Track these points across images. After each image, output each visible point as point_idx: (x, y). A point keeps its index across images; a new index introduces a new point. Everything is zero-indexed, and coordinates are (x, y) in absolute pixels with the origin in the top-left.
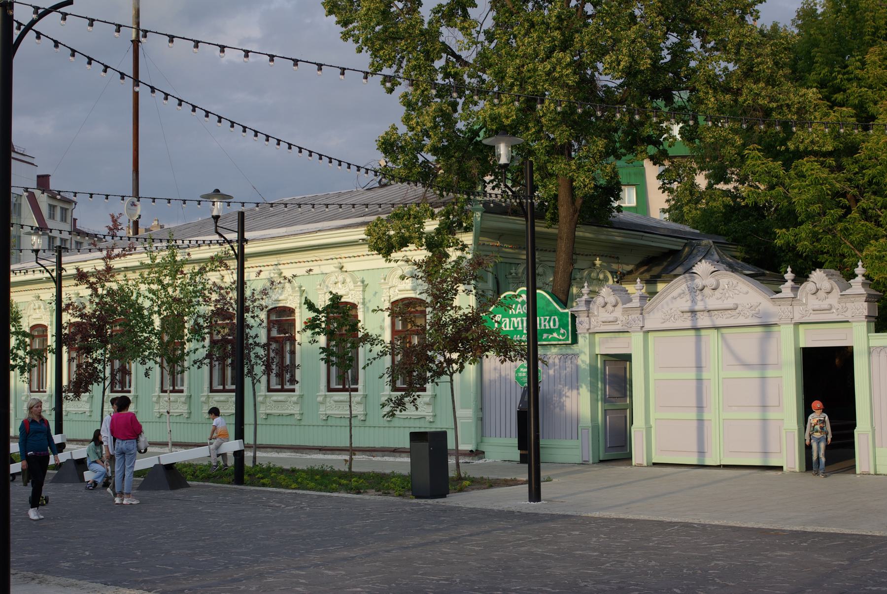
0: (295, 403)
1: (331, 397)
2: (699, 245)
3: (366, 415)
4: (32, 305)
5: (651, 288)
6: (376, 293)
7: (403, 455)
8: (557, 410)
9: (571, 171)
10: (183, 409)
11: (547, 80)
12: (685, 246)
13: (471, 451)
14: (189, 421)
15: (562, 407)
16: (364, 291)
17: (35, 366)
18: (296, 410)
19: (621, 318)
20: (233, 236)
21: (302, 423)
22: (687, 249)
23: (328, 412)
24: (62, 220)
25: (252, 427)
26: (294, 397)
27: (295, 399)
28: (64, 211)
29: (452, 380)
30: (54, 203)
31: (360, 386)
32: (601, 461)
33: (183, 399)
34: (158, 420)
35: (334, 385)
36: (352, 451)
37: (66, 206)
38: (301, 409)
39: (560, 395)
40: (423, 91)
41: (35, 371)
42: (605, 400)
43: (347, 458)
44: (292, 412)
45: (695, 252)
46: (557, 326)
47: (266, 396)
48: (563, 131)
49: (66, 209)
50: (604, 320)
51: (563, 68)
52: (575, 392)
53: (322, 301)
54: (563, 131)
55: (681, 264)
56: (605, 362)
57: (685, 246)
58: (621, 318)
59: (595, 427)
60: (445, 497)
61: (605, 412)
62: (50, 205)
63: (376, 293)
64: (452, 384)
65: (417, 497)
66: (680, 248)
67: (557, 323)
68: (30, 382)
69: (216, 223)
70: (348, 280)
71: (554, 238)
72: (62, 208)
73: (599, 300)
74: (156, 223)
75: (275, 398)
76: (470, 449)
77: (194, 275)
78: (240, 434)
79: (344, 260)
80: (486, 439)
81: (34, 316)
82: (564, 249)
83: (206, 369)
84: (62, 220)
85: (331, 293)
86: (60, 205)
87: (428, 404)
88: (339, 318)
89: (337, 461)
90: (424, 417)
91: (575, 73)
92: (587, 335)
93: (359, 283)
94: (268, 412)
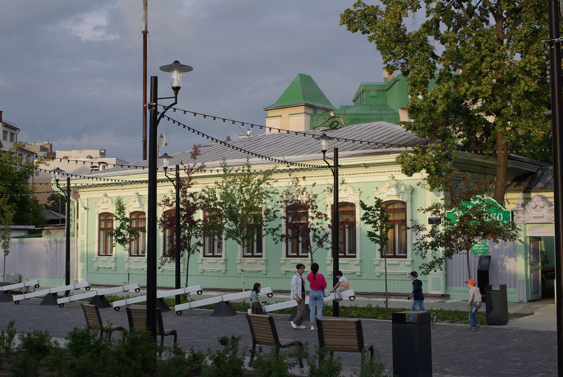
0: (112, 262)
1: (289, 260)
2: (548, 169)
3: (267, 271)
4: (102, 200)
5: (527, 195)
6: (369, 197)
7: (402, 297)
8: (500, 270)
9: (529, 126)
10: (223, 268)
11: (520, 72)
12: (538, 170)
13: (443, 295)
14: (226, 275)
15: (504, 268)
16: (360, 195)
17: (133, 240)
18: (263, 268)
19: (546, 215)
20: (332, 163)
21: (268, 276)
22: (539, 172)
23: (99, 266)
24: (11, 141)
25: (185, 277)
26: (112, 259)
27: (112, 260)
28: (12, 134)
29: (468, 252)
30: (6, 129)
31: (358, 254)
32: (529, 301)
33: (222, 261)
34: (201, 274)
35: (290, 254)
36: (387, 295)
37: (13, 132)
38: (116, 265)
39: (502, 260)
40: (424, 75)
41: (133, 243)
42: (531, 264)
43: (385, 300)
44: (260, 269)
45: (545, 173)
46: (502, 219)
47: (286, 260)
48: (527, 103)
49: (13, 134)
50: (534, 216)
51: (531, 65)
52: (513, 259)
53: (371, 203)
54: (527, 103)
55: (539, 181)
56: (530, 241)
57: (538, 170)
58: (546, 215)
59: (527, 280)
60: (505, 323)
61: (531, 271)
62: (4, 131)
63: (369, 197)
64: (468, 255)
65: (490, 325)
66: (535, 171)
67: (502, 218)
68: (130, 250)
69: (324, 154)
70: (348, 188)
71: (494, 167)
72: (11, 133)
73: (532, 204)
74: (47, 142)
75: (102, 259)
76: (442, 293)
77: (260, 182)
78: (68, 283)
79: (345, 176)
80: (449, 288)
81: (103, 207)
82: (502, 172)
83: (284, 244)
84: (11, 141)
85: (376, 198)
86: (9, 131)
87: (263, 264)
88: (297, 211)
89: (379, 302)
90: (354, 273)
91: (539, 68)
92: (523, 225)
93: (357, 191)
94: (287, 270)
